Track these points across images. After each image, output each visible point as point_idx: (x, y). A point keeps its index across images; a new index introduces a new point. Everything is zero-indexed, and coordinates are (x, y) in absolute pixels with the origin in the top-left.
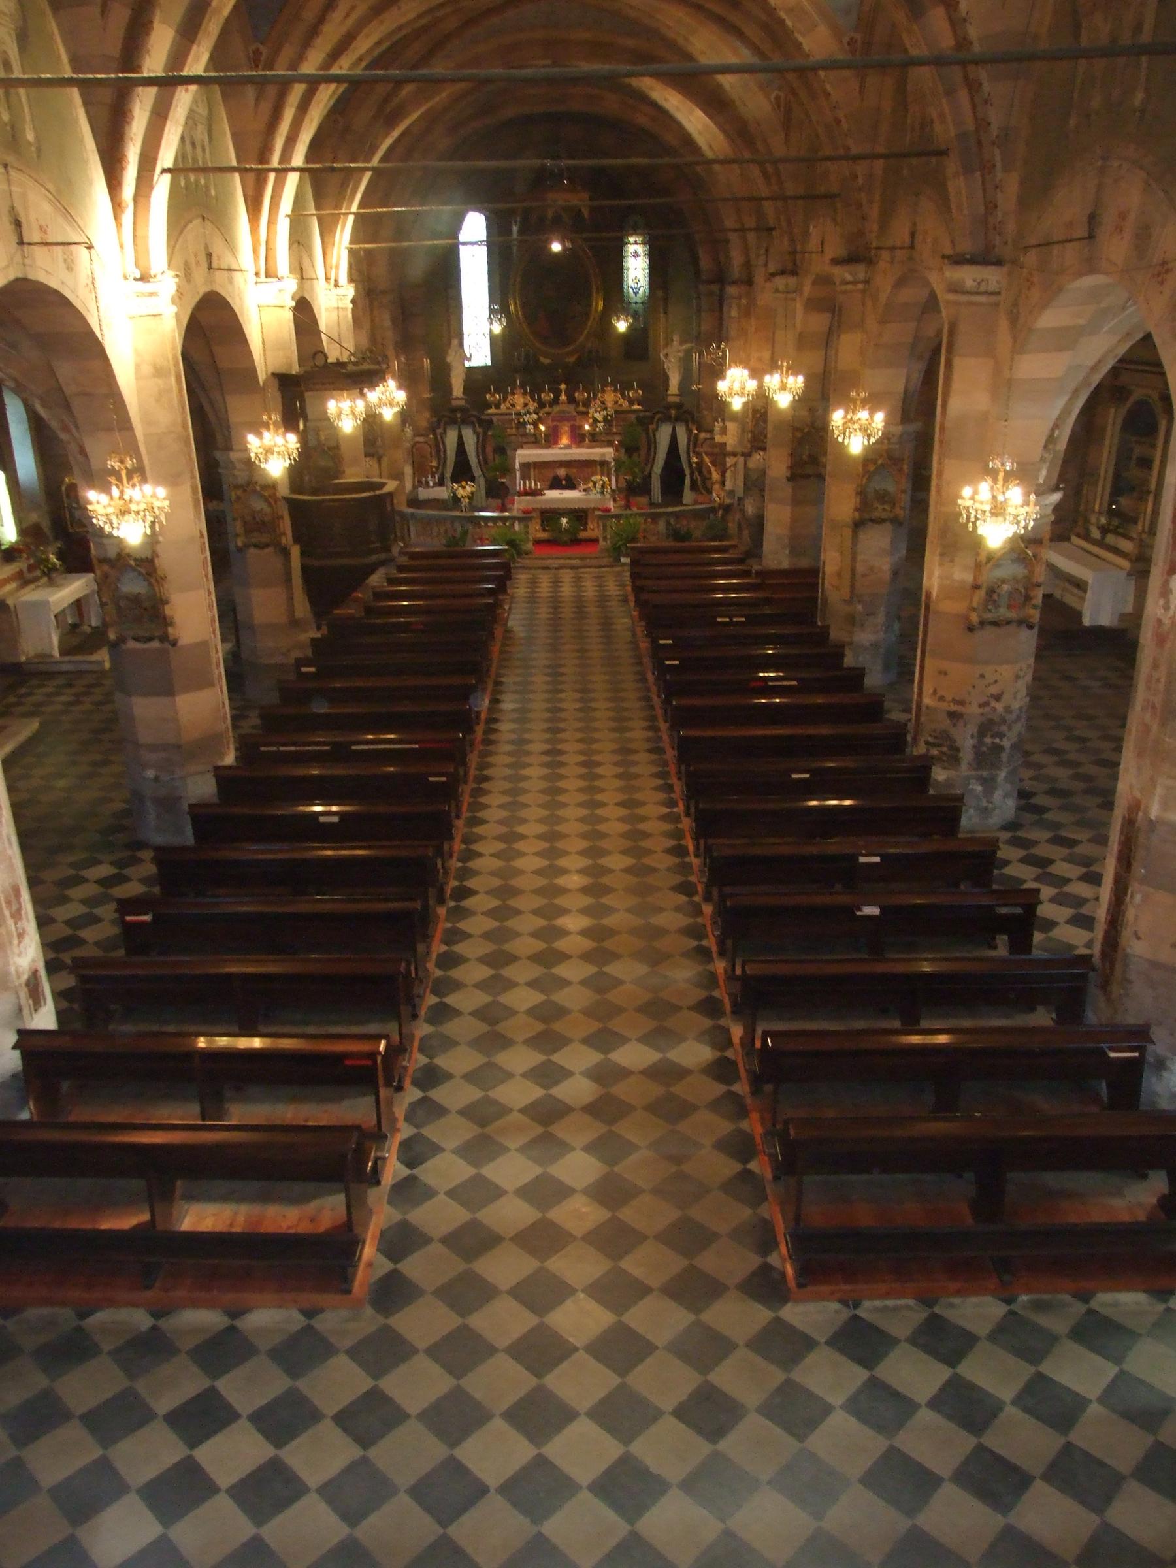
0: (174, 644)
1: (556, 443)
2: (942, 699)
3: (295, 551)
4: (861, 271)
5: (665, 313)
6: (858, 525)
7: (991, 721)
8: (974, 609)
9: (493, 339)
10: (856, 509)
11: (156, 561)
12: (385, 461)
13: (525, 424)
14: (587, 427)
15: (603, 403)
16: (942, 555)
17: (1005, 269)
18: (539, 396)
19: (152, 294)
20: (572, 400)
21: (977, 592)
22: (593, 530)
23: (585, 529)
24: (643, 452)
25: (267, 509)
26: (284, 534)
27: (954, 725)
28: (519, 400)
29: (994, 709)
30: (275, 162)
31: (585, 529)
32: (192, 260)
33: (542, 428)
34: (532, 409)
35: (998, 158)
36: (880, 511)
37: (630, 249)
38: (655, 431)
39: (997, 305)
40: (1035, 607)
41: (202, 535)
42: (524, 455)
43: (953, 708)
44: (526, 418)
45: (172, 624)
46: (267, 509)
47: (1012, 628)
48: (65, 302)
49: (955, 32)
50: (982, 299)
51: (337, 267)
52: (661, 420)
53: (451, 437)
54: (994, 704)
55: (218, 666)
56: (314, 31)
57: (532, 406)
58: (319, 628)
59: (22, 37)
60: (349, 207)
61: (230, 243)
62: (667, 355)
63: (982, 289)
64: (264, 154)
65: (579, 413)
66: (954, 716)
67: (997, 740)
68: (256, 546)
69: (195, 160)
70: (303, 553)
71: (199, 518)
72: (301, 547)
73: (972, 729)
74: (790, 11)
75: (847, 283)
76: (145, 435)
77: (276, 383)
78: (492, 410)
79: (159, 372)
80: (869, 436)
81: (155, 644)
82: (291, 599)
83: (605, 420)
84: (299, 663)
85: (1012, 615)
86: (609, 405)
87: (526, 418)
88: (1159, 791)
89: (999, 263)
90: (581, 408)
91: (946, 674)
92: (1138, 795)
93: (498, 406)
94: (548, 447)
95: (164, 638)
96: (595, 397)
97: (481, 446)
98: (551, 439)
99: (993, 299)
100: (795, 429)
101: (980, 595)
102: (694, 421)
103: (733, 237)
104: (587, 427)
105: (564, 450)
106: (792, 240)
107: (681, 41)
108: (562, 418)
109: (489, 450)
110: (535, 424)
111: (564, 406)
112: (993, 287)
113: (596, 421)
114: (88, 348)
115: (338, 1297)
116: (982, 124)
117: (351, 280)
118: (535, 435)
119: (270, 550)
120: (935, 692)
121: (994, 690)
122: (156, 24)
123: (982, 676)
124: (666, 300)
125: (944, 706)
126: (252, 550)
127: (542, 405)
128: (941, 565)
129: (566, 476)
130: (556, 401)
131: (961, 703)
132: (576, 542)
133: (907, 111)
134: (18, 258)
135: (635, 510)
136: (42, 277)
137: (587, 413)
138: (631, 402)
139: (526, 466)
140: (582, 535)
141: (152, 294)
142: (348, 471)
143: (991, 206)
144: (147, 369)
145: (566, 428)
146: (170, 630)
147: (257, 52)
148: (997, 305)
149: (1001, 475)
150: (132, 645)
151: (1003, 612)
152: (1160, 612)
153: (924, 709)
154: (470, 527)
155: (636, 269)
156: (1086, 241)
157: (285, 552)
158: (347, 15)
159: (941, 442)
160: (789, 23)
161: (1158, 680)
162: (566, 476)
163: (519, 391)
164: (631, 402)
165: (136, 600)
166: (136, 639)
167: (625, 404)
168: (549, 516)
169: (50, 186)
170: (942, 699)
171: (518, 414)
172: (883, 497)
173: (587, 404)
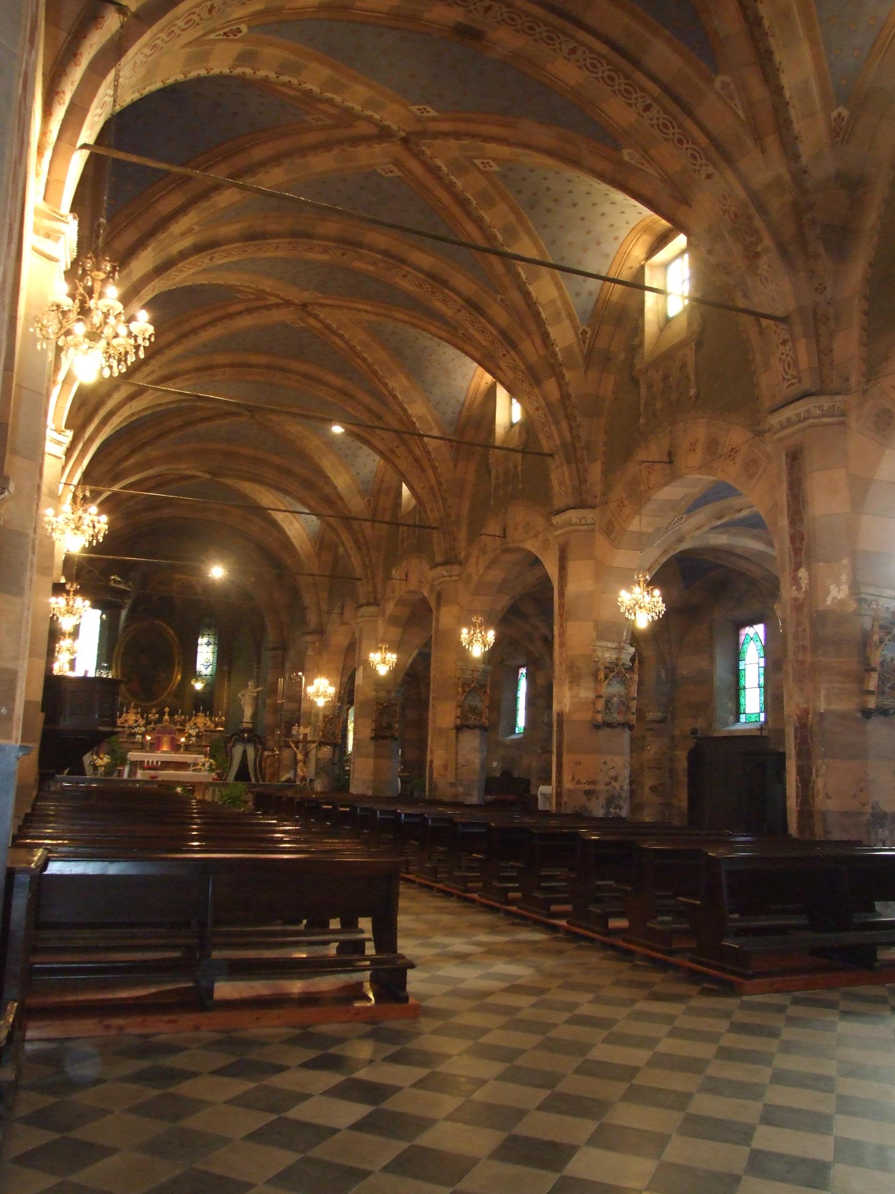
2: (579, 782)
4: (456, 570)
5: (229, 680)
6: (459, 729)
7: (613, 796)
8: (599, 712)
10: (457, 717)
13: (134, 734)
15: (195, 724)
16: (571, 682)
17: (597, 510)
18: (147, 717)
20: (173, 722)
27: (590, 800)
29: (614, 788)
33: (148, 738)
35: (586, 456)
36: (472, 720)
37: (202, 640)
38: (231, 748)
39: (593, 531)
40: (633, 714)
42: (134, 756)
43: (587, 787)
44: (136, 730)
47: (619, 729)
49: (561, 390)
54: (614, 784)
57: (142, 722)
62: (243, 695)
63: (583, 521)
66: (589, 793)
67: (618, 811)
72: (46, 716)
73: (602, 801)
74: (419, 418)
75: (444, 577)
80: (485, 646)
85: (620, 718)
87: (136, 730)
88: (823, 693)
89: (592, 507)
91: (580, 763)
92: (805, 706)
96: (190, 720)
98: (155, 746)
99: (592, 527)
100: (378, 704)
101: (600, 704)
102: (261, 742)
104: (183, 740)
106: (374, 585)
108: (165, 731)
110: (143, 735)
113: (190, 736)
115: (396, 1006)
116: (575, 438)
118: (142, 743)
120: (573, 778)
121: (612, 773)
123: (605, 763)
124: (230, 673)
125: (581, 787)
127: (148, 723)
128: (570, 689)
130: (160, 721)
131: (594, 783)
133: (489, 471)
137: (183, 731)
143: (582, 481)
145: (166, 739)
148: (593, 531)
151: (616, 717)
152: (794, 593)
153: (564, 792)
156: (667, 465)
158: (149, 375)
159: (561, 615)
160: (417, 425)
161: (804, 630)
163: (132, 711)
164: (216, 726)
167: (213, 726)
170: (579, 782)
171: (131, 727)
172: (474, 710)
173: (183, 724)
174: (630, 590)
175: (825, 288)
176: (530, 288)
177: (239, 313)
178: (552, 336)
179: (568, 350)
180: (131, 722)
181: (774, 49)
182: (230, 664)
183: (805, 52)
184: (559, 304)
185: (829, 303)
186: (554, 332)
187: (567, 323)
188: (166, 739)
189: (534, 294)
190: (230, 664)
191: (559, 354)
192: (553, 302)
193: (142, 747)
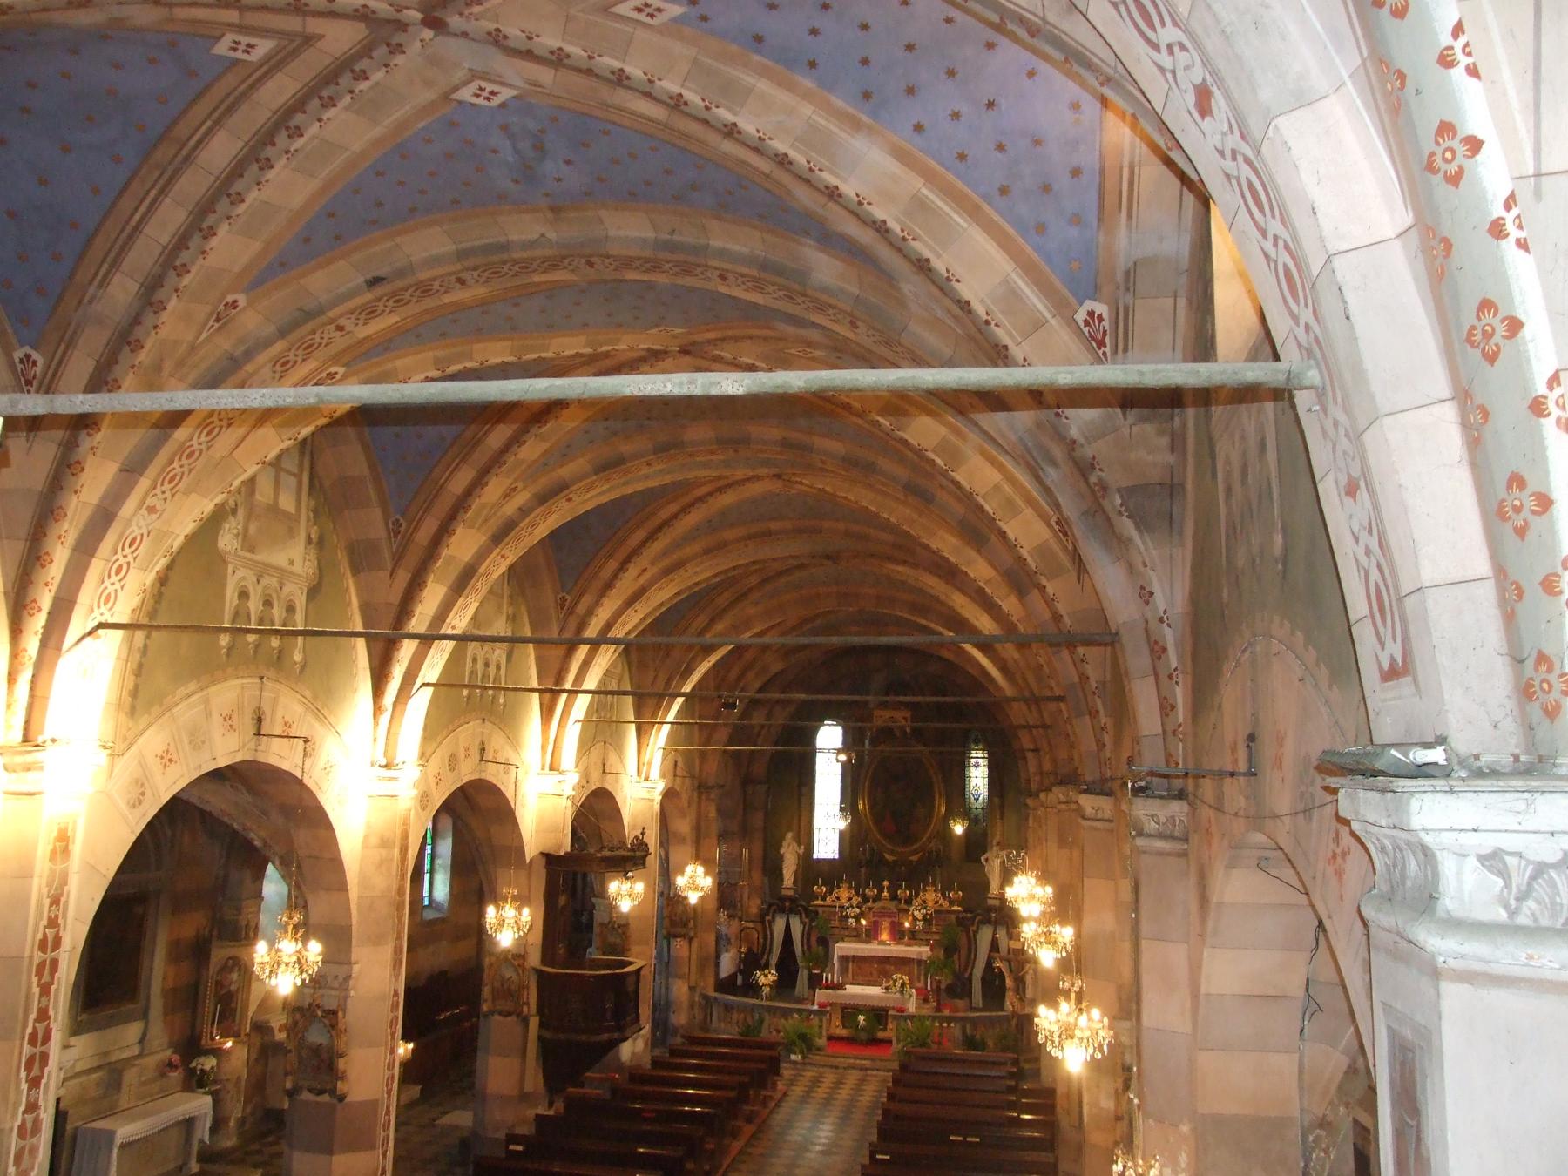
0: (341, 1099)
1: (876, 938)
3: (534, 1022)
9: (841, 833)
11: (340, 1014)
12: (695, 944)
13: (847, 917)
14: (907, 925)
19: (391, 779)
20: (894, 897)
21: (1119, 1124)
22: (890, 1032)
23: (885, 1029)
24: (964, 952)
25: (515, 977)
26: (527, 1004)
28: (844, 893)
30: (568, 686)
31: (885, 1029)
32: (462, 753)
33: (864, 922)
34: (855, 902)
38: (975, 933)
41: (396, 994)
42: (843, 948)
45: (342, 1078)
46: (515, 977)
48: (300, 782)
50: (1098, 825)
51: (650, 764)
52: (982, 922)
53: (779, 925)
55: (386, 1127)
56: (609, 586)
58: (551, 1105)
59: (313, 592)
60: (665, 716)
61: (514, 740)
64: (560, 677)
65: (900, 910)
68: (500, 1014)
69: (485, 676)
70: (542, 1025)
71: (397, 976)
76: (360, 897)
77: (543, 861)
78: (819, 902)
79: (384, 843)
81: (326, 1098)
82: (523, 1071)
83: (924, 918)
84: (512, 1138)
86: (930, 904)
90: (903, 906)
93: (824, 899)
94: (867, 942)
95: (333, 1092)
96: (917, 896)
97: (806, 936)
98: (871, 934)
103: (1030, 755)
105: (885, 946)
107: (943, 597)
108: (884, 913)
109: (813, 940)
110: (857, 918)
111: (886, 902)
112: (1108, 814)
113: (915, 919)
114: (317, 819)
117: (663, 775)
119: (513, 1019)
122: (429, 583)
124: (1002, 807)
126: (497, 1017)
127: (865, 899)
129: (880, 968)
132: (874, 1042)
134: (252, 745)
135: (946, 1013)
136: (273, 760)
138: (952, 903)
139: (844, 959)
140: (881, 1035)
141: (391, 779)
142: (635, 949)
144: (374, 840)
145: (886, 924)
146: (339, 1084)
147: (563, 599)
149: (1073, 996)
150: (306, 1096)
154: (767, 1017)
155: (978, 777)
157: (525, 1021)
160: (988, 591)
162: (880, 968)
163: (844, 886)
164: (952, 903)
165: (316, 1050)
166: (310, 1091)
167: (946, 904)
168: (849, 1012)
169: (307, 693)
171: (842, 907)
173: (909, 902)
174: (1054, 1004)
175: (1151, 594)
176: (957, 476)
177: (675, 516)
178: (1011, 535)
179: (1042, 551)
180: (844, 901)
181: (927, 253)
182: (1002, 797)
183: (980, 240)
184: (1008, 489)
185: (1161, 620)
186: (1012, 529)
187: (1029, 512)
188: (886, 924)
189: (964, 483)
190: (1002, 797)
191: (1029, 560)
192: (997, 487)
193: (856, 935)
